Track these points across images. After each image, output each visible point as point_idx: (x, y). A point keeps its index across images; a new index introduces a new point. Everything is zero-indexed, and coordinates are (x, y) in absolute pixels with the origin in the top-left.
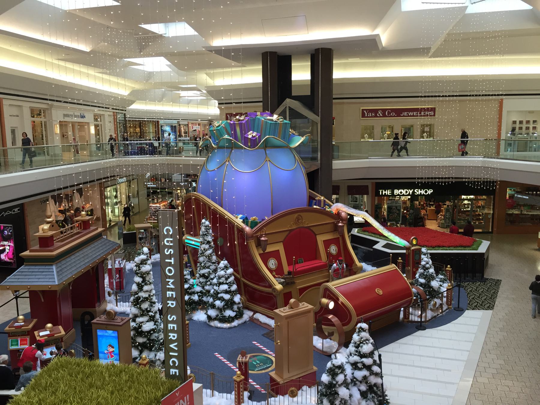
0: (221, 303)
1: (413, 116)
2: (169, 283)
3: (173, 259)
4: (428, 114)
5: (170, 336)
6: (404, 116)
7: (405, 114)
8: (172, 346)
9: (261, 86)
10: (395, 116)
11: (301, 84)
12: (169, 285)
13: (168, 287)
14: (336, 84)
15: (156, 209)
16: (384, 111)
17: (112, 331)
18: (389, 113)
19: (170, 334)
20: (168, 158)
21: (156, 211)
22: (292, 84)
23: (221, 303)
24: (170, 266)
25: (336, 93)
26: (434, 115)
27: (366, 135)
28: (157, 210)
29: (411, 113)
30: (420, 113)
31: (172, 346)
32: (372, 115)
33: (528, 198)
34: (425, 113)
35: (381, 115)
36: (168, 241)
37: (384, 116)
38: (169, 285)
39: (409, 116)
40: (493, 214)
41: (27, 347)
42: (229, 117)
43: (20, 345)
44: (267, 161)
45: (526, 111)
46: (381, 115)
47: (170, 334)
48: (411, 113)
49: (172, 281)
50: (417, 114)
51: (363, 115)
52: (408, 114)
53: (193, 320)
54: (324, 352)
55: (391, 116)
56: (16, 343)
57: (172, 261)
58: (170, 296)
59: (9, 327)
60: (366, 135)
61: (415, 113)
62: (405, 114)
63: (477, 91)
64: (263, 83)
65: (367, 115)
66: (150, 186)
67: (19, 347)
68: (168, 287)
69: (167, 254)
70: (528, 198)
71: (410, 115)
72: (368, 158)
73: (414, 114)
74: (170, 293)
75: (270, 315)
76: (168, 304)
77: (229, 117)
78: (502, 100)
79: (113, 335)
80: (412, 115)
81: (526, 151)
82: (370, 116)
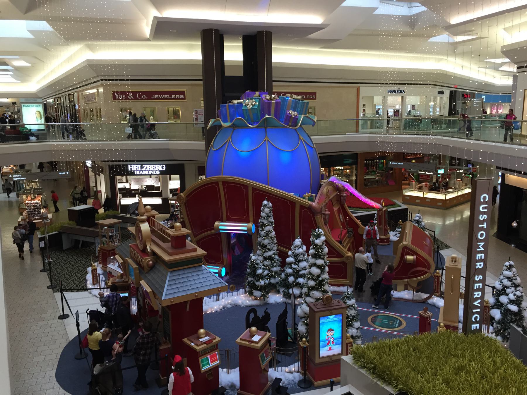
0: (304, 279)
1: (164, 99)
2: (480, 247)
3: (485, 223)
4: (179, 97)
5: (475, 295)
6: (155, 99)
7: (156, 96)
8: (476, 303)
9: (242, 64)
10: (146, 99)
11: (234, 65)
12: (479, 248)
13: (478, 250)
14: (274, 67)
15: (35, 206)
16: (135, 93)
17: (333, 316)
18: (140, 96)
19: (475, 293)
20: (77, 143)
21: (36, 209)
22: (225, 64)
23: (304, 279)
24: (482, 231)
25: (275, 76)
26: (315, 99)
27: (151, 117)
28: (36, 207)
29: (161, 96)
30: (171, 96)
31: (476, 303)
32: (123, 97)
33: (402, 164)
34: (175, 97)
35: (132, 98)
36: (483, 208)
37: (135, 98)
38: (479, 248)
39: (159, 99)
40: (356, 180)
41: (218, 362)
42: (117, 96)
43: (211, 363)
44: (265, 140)
45: (370, 97)
46: (132, 98)
47: (475, 293)
48: (161, 96)
49: (482, 244)
50: (168, 97)
51: (114, 98)
52: (159, 97)
53: (269, 304)
54: (415, 301)
55: (142, 99)
56: (206, 362)
57: (485, 226)
58: (480, 258)
59: (241, 339)
60: (151, 117)
61: (165, 96)
62: (156, 97)
63: (400, 80)
64: (244, 61)
65: (118, 97)
66: (17, 179)
67: (211, 366)
68: (478, 250)
69: (482, 219)
70: (402, 164)
71: (161, 98)
72: (346, 134)
73: (165, 97)
74: (480, 255)
75: (332, 283)
76: (476, 265)
77: (117, 96)
78: (359, 87)
79: (335, 319)
80: (163, 98)
81: (373, 129)
82: (122, 98)
